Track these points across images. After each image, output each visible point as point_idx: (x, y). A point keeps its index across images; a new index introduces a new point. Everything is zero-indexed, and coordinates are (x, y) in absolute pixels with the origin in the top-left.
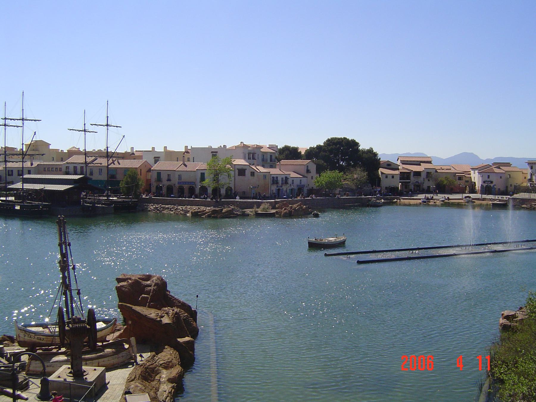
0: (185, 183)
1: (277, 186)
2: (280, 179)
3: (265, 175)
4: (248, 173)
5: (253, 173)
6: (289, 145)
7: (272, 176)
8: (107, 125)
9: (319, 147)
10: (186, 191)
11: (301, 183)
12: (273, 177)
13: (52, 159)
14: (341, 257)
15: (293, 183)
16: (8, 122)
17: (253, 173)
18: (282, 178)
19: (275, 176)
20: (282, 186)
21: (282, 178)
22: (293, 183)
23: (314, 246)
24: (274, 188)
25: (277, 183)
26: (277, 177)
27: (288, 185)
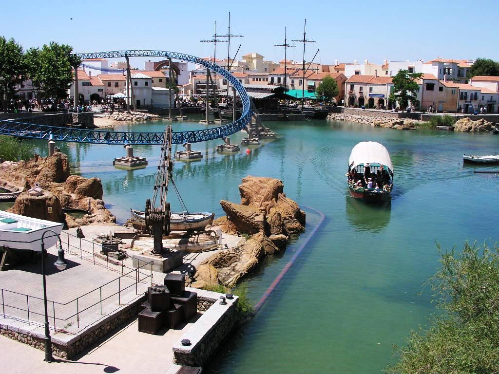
0: (375, 95)
1: (466, 102)
2: (469, 95)
3: (454, 91)
4: (436, 88)
5: (442, 87)
6: (482, 58)
7: (461, 91)
8: (285, 45)
9: (93, 122)
10: (376, 103)
11: (491, 99)
12: (462, 93)
13: (264, 70)
14: (489, 175)
15: (483, 99)
16: (217, 38)
17: (442, 87)
18: (472, 94)
19: (464, 92)
20: (470, 102)
21: (472, 94)
22: (483, 99)
23: (468, 163)
24: (462, 103)
25: (466, 98)
26: (466, 93)
27: (478, 101)
